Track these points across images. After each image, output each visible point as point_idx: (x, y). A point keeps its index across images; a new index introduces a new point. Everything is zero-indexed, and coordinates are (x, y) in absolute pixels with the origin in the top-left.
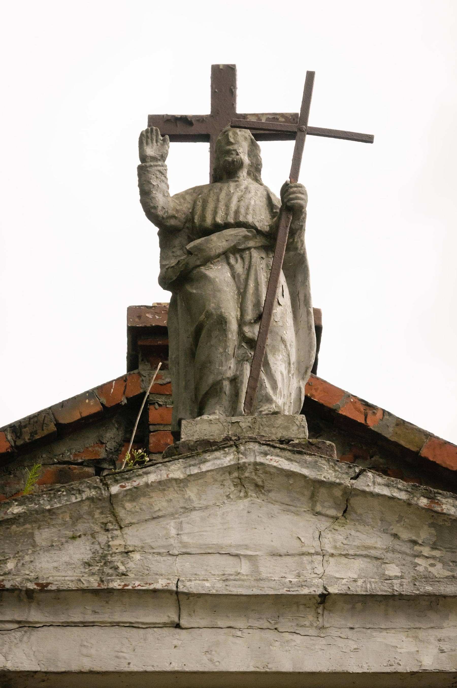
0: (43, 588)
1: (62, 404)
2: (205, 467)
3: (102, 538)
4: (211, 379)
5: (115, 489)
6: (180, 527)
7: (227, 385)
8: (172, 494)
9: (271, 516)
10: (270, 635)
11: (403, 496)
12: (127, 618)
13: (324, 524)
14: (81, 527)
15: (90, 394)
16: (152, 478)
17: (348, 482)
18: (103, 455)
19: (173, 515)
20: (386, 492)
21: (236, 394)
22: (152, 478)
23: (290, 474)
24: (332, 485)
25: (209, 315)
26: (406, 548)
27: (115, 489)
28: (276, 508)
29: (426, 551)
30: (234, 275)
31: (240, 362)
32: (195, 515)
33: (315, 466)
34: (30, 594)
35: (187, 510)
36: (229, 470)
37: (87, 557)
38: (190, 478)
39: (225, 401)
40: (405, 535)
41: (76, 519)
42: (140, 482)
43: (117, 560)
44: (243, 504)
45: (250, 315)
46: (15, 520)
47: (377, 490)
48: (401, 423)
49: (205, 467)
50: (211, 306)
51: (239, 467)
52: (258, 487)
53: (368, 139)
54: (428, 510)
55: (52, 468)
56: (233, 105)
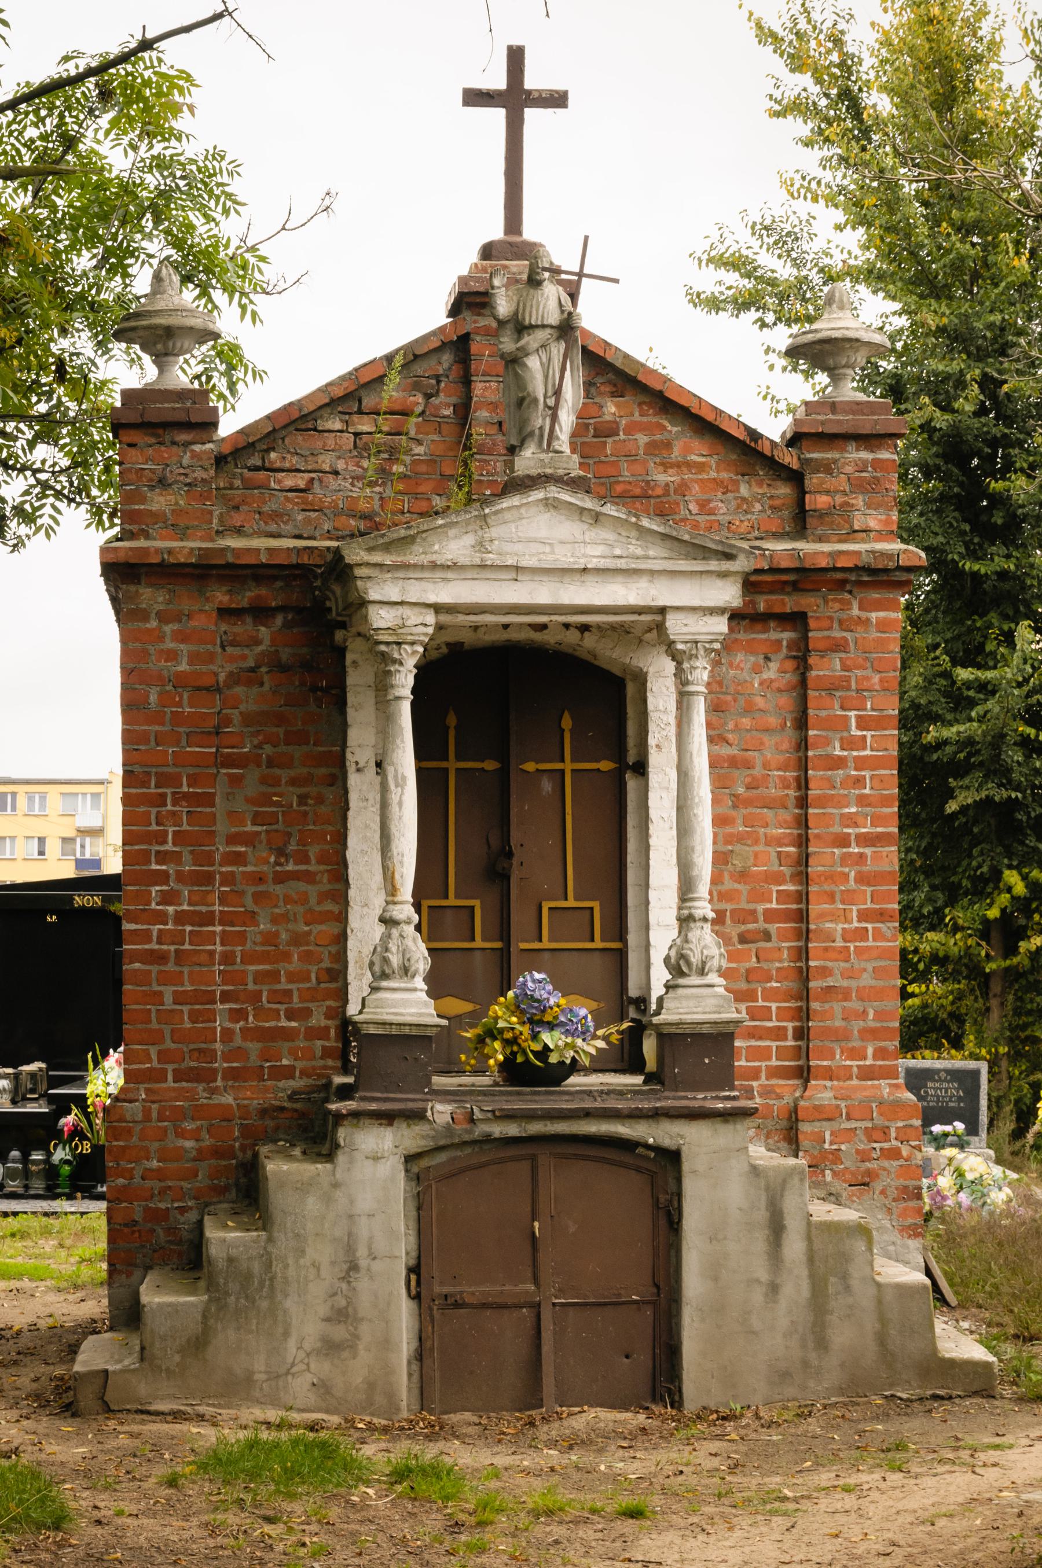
0: (455, 564)
1: (417, 341)
2: (530, 499)
3: (480, 533)
4: (529, 429)
5: (487, 511)
6: (517, 527)
7: (537, 432)
8: (514, 512)
9: (560, 522)
10: (558, 585)
11: (624, 516)
12: (493, 576)
13: (586, 526)
14: (470, 528)
15: (433, 333)
16: (505, 505)
17: (598, 509)
18: (441, 372)
19: (513, 521)
20: (616, 514)
21: (541, 436)
22: (505, 505)
23: (571, 504)
24: (590, 510)
25: (529, 394)
26: (624, 540)
27: (487, 511)
28: (563, 518)
29: (634, 541)
30: (542, 363)
31: (544, 419)
32: (524, 521)
33: (582, 500)
34: (448, 567)
35: (520, 519)
36: (541, 500)
37: (473, 543)
38: (522, 505)
39: (536, 439)
40: (624, 534)
41: (467, 524)
42: (499, 507)
43: (487, 545)
44: (547, 515)
45: (550, 394)
46: (440, 526)
47: (613, 513)
48: (626, 356)
49: (530, 499)
50: (530, 389)
51: (546, 499)
52: (555, 507)
53: (616, 281)
54: (636, 524)
55: (409, 380)
56: (522, 83)
